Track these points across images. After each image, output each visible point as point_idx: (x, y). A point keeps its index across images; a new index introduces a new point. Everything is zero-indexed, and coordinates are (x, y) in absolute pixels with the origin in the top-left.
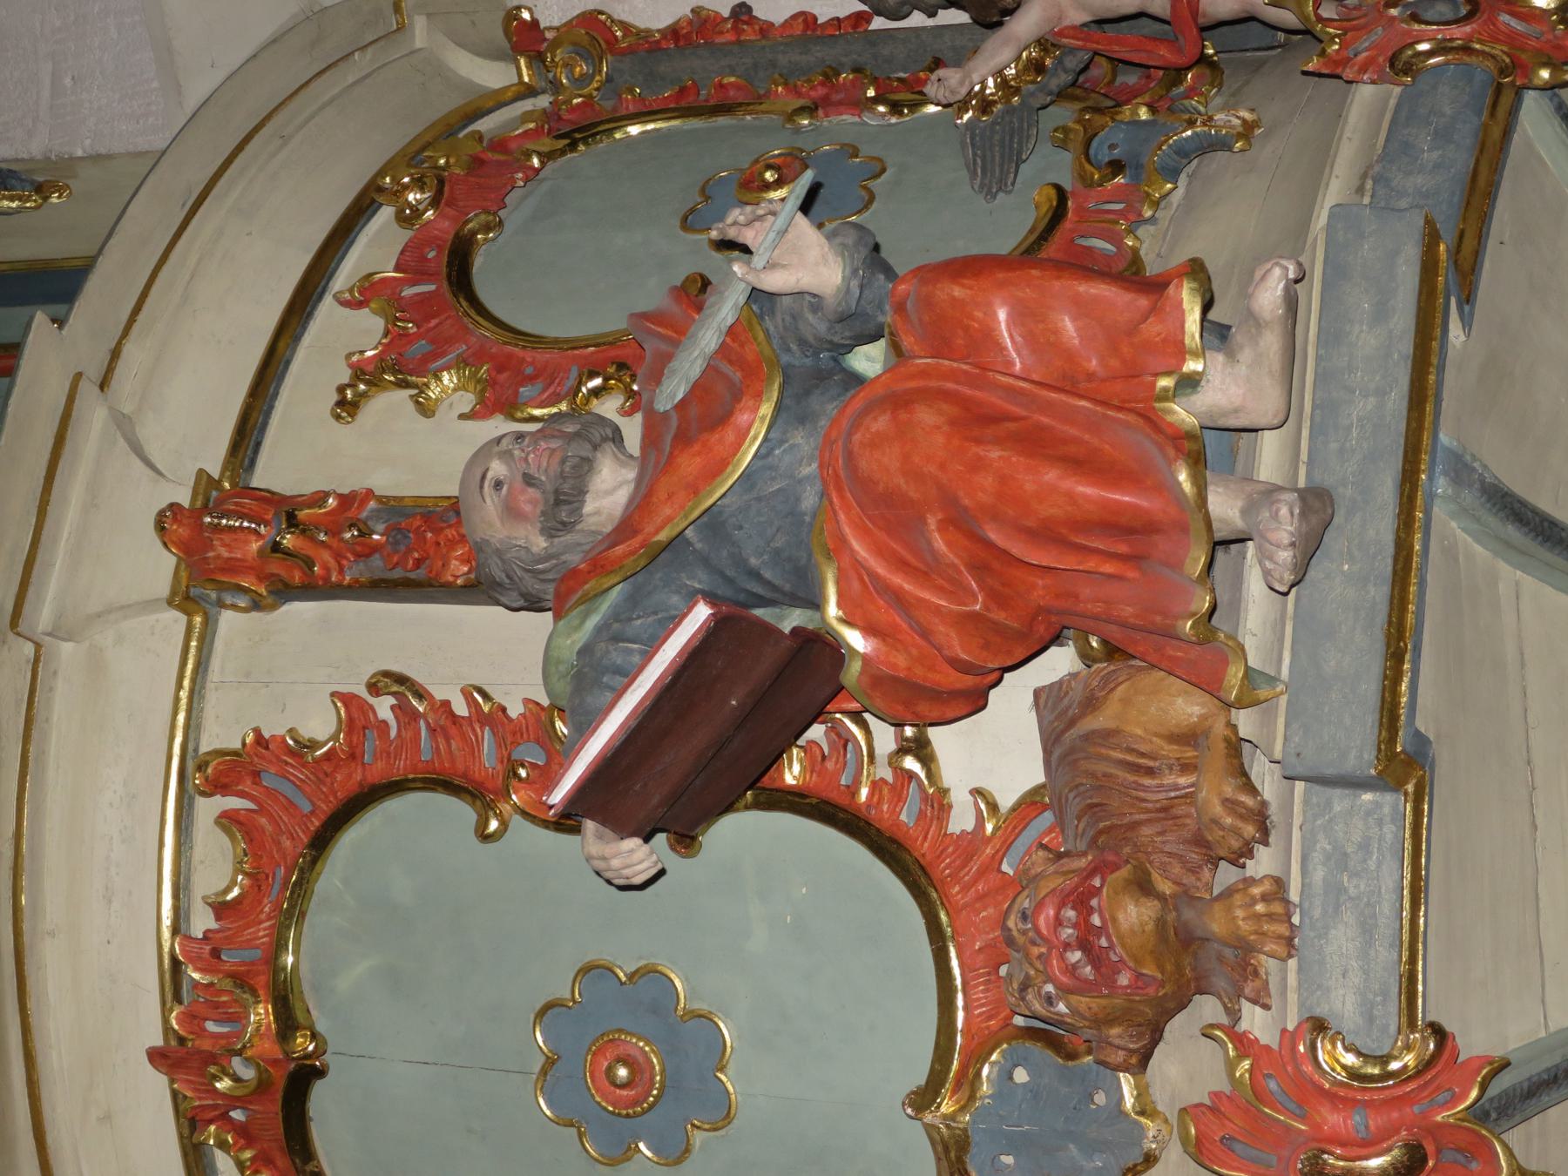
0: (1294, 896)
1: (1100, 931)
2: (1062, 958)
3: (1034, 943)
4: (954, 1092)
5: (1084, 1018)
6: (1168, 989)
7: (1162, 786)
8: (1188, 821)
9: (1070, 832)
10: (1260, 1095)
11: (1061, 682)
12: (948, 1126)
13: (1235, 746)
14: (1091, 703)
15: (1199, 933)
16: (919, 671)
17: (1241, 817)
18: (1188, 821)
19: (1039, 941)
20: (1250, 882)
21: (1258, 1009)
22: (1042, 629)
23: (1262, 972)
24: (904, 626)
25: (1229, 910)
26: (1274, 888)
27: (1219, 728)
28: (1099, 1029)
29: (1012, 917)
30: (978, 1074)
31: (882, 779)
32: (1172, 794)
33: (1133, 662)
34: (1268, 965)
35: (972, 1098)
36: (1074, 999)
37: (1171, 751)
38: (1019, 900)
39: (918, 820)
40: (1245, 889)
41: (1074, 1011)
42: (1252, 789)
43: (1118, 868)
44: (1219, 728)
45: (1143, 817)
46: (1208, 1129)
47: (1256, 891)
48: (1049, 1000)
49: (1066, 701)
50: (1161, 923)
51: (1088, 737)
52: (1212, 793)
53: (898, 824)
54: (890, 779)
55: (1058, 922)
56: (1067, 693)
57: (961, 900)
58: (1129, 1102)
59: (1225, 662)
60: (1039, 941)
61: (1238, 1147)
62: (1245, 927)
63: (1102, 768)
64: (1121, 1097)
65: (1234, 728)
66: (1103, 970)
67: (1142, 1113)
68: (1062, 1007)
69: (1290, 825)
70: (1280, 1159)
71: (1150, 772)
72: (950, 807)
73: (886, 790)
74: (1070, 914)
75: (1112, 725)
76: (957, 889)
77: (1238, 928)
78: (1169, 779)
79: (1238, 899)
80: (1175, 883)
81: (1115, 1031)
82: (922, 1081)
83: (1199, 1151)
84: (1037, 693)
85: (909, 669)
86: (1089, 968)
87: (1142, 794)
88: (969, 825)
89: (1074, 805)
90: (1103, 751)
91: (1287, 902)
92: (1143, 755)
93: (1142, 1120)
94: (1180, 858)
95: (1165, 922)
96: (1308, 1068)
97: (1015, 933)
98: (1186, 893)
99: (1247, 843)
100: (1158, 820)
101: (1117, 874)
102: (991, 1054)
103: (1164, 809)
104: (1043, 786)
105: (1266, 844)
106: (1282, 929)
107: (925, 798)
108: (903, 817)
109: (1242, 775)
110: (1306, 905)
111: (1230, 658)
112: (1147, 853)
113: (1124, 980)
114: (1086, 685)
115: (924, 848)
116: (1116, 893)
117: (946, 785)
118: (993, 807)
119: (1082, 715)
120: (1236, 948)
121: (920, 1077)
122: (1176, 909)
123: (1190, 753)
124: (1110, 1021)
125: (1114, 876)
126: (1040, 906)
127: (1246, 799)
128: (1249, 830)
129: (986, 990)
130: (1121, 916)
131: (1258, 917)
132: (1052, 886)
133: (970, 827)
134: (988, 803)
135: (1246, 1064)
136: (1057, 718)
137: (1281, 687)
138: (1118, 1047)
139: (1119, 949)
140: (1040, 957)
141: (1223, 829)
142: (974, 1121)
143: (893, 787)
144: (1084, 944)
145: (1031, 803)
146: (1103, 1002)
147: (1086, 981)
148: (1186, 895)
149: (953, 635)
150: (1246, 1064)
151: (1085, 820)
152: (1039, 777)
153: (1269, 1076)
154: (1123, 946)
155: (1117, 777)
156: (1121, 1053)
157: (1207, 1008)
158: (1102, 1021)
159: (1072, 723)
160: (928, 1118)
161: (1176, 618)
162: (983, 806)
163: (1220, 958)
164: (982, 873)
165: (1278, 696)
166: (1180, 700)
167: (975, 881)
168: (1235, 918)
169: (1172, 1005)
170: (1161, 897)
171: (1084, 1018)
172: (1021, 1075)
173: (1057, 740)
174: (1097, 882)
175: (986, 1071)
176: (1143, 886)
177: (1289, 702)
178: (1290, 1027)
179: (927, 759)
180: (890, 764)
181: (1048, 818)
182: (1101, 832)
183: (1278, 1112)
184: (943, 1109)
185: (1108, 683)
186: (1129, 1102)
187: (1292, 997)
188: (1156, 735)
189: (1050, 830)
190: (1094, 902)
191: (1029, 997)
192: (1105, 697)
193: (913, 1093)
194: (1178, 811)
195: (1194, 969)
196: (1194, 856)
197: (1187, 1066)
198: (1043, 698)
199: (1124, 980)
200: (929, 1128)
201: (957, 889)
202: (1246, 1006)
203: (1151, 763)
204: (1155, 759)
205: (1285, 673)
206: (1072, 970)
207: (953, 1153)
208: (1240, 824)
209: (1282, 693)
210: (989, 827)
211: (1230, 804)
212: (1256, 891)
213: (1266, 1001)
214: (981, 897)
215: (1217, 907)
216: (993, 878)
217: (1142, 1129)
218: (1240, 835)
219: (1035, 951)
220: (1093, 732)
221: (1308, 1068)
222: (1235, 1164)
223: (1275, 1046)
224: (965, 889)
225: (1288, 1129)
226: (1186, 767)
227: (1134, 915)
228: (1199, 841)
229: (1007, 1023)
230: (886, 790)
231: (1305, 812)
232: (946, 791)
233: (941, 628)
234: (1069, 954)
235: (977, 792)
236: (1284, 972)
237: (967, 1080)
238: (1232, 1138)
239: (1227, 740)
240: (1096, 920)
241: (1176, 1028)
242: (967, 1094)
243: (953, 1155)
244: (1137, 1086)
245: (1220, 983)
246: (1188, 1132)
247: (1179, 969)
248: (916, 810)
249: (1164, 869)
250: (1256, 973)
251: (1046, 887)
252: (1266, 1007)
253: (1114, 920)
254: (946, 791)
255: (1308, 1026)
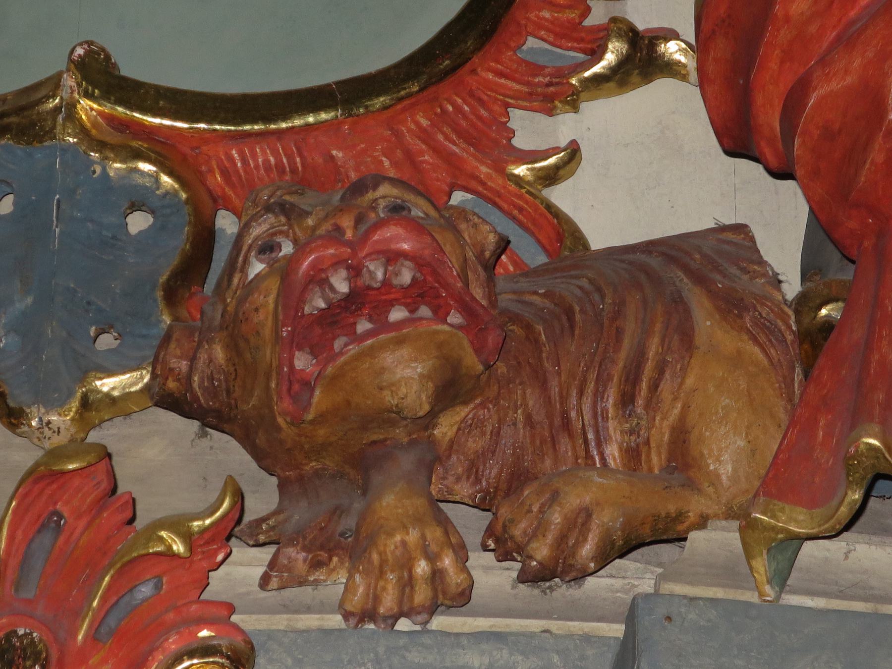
0: (439, 622)
1: (382, 326)
2: (338, 263)
3: (359, 220)
4: (111, 120)
5: (242, 301)
6: (288, 432)
7: (605, 419)
8: (548, 462)
9: (524, 284)
10: (130, 571)
11: (762, 262)
12: (57, 110)
13: (669, 532)
14: (731, 307)
15: (377, 479)
16: (784, 35)
17: (562, 538)
18: (548, 462)
19: (363, 228)
20: (461, 552)
21: (260, 571)
22: (852, 224)
23: (320, 575)
24: (852, 14)
25: (418, 521)
26: (453, 590)
27: (696, 505)
28: (222, 327)
29: (395, 192)
30: (139, 156)
31: (588, 10)
32: (591, 436)
33: (798, 370)
34: (335, 583)
35: (101, 146)
36: (274, 284)
37: (661, 432)
38: (421, 201)
39: (528, 64)
40: (451, 546)
41: (251, 287)
42: (609, 553)
43: (478, 351)
44: (696, 505)
45: (555, 391)
46: (77, 497)
47: (447, 562)
48: (268, 248)
49: (734, 270)
50: (391, 416)
51: (679, 303)
52: (599, 494)
53: (521, 34)
54: (588, 22)
55: (392, 257)
56: (745, 271)
57: (408, 127)
58: (107, 384)
59: (811, 504)
60: (363, 228)
61: (46, 539)
62: (392, 544)
63: (631, 327)
64: (111, 374)
65: (702, 523)
66: (318, 330)
67: (86, 404)
68: (257, 267)
69: (548, 616)
70: (29, 602)
71: (626, 400)
72: (550, 112)
73: (572, 15)
74: (406, 276)
75: (700, 339)
76: (424, 122)
77: (390, 534)
78: (613, 427)
79: (434, 534)
80: (452, 442)
81: (220, 353)
82: (126, 71)
83: (43, 478)
84: (741, 229)
85: (787, 19)
86: (322, 305)
87: (591, 386)
88: (520, 142)
89: (570, 289)
90: (658, 327)
91: (432, 610)
92: (654, 387)
93: (75, 404)
94: (491, 451)
95: (393, 424)
96: (173, 644)
97: (370, 196)
98: (438, 459)
99: (520, 549)
100: (550, 416)
101: (469, 349)
102: (170, 174)
103: (566, 423)
104: (586, 246)
105: (524, 577)
106: (388, 602)
107: (562, 74)
108: (532, 42)
109: (627, 547)
110: (426, 640)
111: (817, 511)
112: (498, 396)
113: (302, 361)
114: (762, 299)
115: (485, 72)
116: (440, 346)
117: (584, 106)
118: (551, 177)
119: (713, 294)
120: (358, 531)
121: (130, 67)
122: (412, 443)
123: (657, 460)
124: (234, 347)
125: (466, 343)
126: (417, 227)
127: (587, 549)
128: (541, 551)
129: (267, 167)
130: (405, 352)
131: (406, 565)
132: (447, 249)
133: (517, 142)
134: (557, 167)
135: (179, 547)
136: (704, 256)
137: (770, 592)
138: (193, 360)
139: (353, 349)
140: (338, 229)
141: (541, 511)
142: (66, 149)
143: (576, 26)
144: (357, 301)
145: (562, 234)
146: (267, 332)
147: (301, 301)
148: (433, 459)
149: (849, 80)
150: (179, 547)
151: (547, 303)
152: (597, 241)
153: (158, 587)
154: (358, 357)
155: (617, 349)
156: (184, 365)
157: (263, 497)
158: (235, 332)
159: (699, 279)
160: (69, 81)
161: (883, 423)
162: (552, 160)
163: (338, 512)
164: (451, 162)
165: (758, 588)
166: (741, 443)
167: (437, 150)
168: (405, 527)
169: (261, 439)
170: (431, 418)
171: (242, 301)
172: (138, 222)
173: (671, 259)
174: (455, 318)
175: (145, 167)
176: (450, 389)
177: (748, 605)
178: (235, 618)
179: (619, 78)
180: (614, 20)
181: (536, 258)
182: (528, 327)
183: (104, 599)
184: (85, 103)
185: (764, 332)
186: (107, 384)
187: (281, 622)
188: (686, 408)
189: (517, 262)
190: (424, 311)
191: (271, 218)
192: (743, 329)
193: (108, 57)
194: (565, 445)
195: (317, 473)
196: (492, 471)
197: (172, 467)
198: (735, 242)
199: (302, 361)
200: (54, 83)
201: (424, 122)
202: (266, 554)
203: (640, 402)
204: (647, 407)
205: (792, 600)
206: (318, 279)
207: (17, 119)
208: (550, 538)
209: (761, 594)
210: (521, 170)
211: (581, 520)
212: (447, 562)
213: (274, 583)
214: (410, 157)
215: (419, 503)
216: (439, 177)
217: (59, 404)
218: (534, 536)
219: (347, 222)
220: (687, 311)
221: (173, 644)
222: (19, 535)
223: (205, 596)
224: (425, 135)
225: (77, 615)
226: (633, 456)
227: (405, 374)
228: (518, 479)
229: (219, 202)
230: (572, 15)
231: (570, 636)
232: (575, 107)
233: (857, 63)
234: (343, 273)
235: (573, 152)
236: (321, 609)
237: (133, 142)
238: (58, 528)
239: (680, 516)
240: (397, 314)
241: (229, 454)
242: (108, 139)
243: (13, 119)
244: (127, 396)
245: (300, 514)
246: (70, 458)
247: (319, 450)
248: (541, 61)
249: (466, 428)
250: (316, 565)
251: (446, 241)
252: (264, 582)
253: (399, 342)
254: (575, 107)
255: (239, 641)
